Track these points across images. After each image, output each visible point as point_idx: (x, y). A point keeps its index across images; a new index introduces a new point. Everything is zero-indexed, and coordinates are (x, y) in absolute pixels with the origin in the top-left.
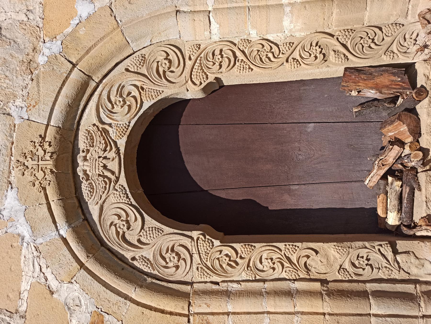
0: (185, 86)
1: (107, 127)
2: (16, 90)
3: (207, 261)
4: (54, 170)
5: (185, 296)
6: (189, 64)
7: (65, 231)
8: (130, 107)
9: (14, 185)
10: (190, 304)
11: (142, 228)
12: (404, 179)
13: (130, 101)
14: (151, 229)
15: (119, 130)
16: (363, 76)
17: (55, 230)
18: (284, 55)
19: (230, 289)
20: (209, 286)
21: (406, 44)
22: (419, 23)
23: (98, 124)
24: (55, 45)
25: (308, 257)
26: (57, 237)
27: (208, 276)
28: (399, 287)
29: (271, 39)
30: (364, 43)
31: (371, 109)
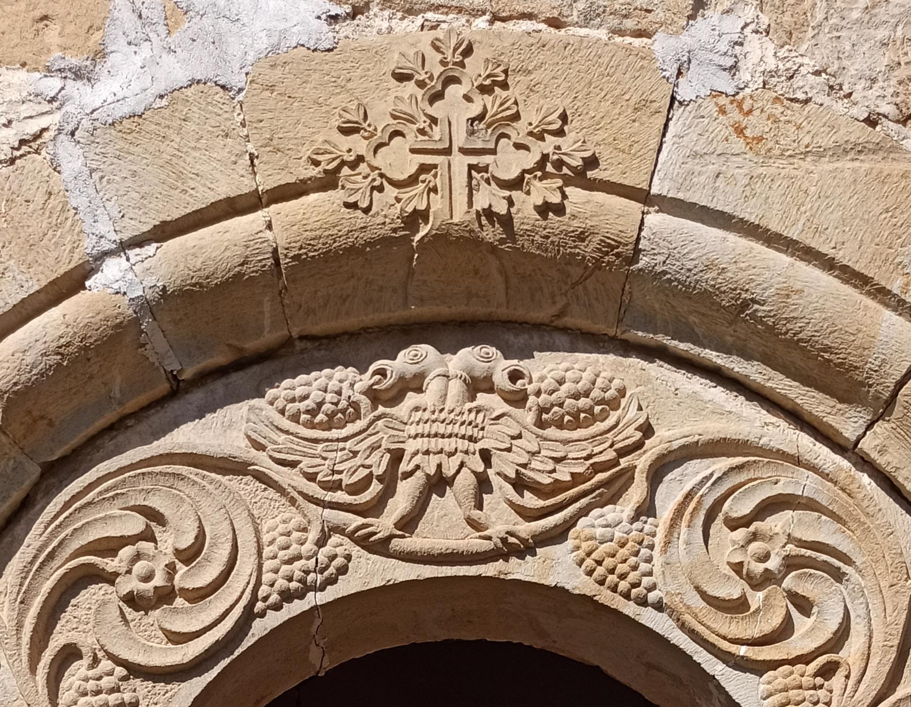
1: (636, 493)
2: (823, 38)
4: (424, 231)
9: (345, 29)
17: (126, 236)
26: (89, 245)
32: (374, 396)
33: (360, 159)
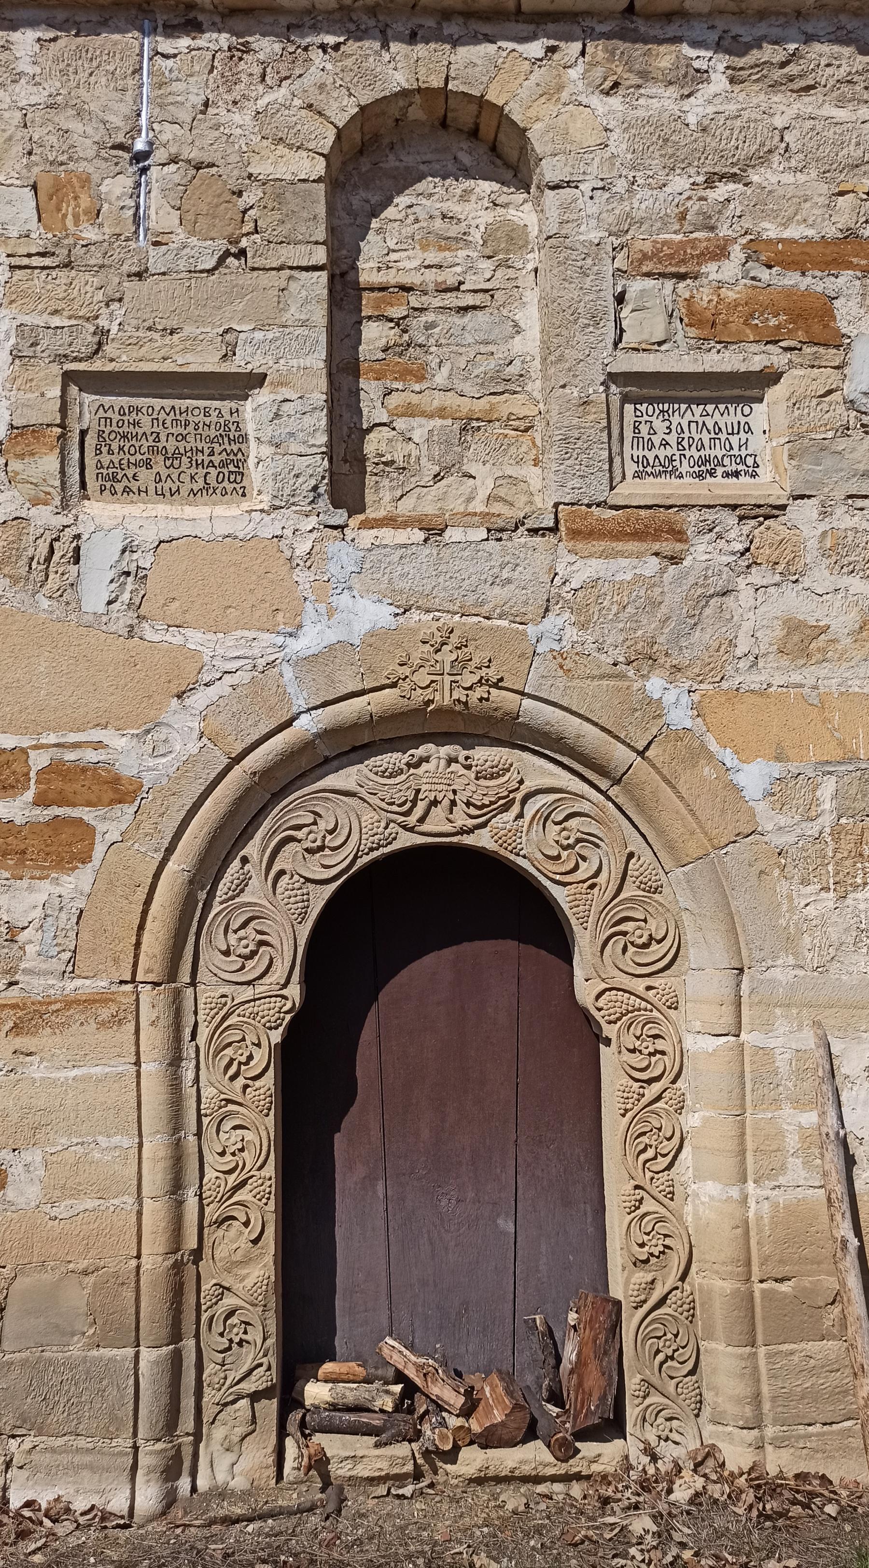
0: (595, 974)
1: (515, 809)
2: (597, 628)
3: (239, 1015)
4: (431, 707)
5: (172, 975)
6: (639, 985)
7: (307, 725)
8: (559, 857)
9: (401, 619)
10: (156, 984)
11: (308, 880)
12: (399, 1416)
13: (568, 859)
14: (305, 897)
15: (510, 834)
16: (602, 1337)
17: (310, 706)
18: (648, 1182)
19: (183, 1064)
20: (188, 1020)
21: (660, 1420)
22: (698, 1445)
23: (524, 789)
24: (682, 715)
25: (246, 1224)
26: (295, 710)
27: (209, 1018)
28: (188, 1403)
29: (683, 1156)
30: (666, 1340)
31: (540, 1352)
32: (409, 765)
33: (407, 677)
